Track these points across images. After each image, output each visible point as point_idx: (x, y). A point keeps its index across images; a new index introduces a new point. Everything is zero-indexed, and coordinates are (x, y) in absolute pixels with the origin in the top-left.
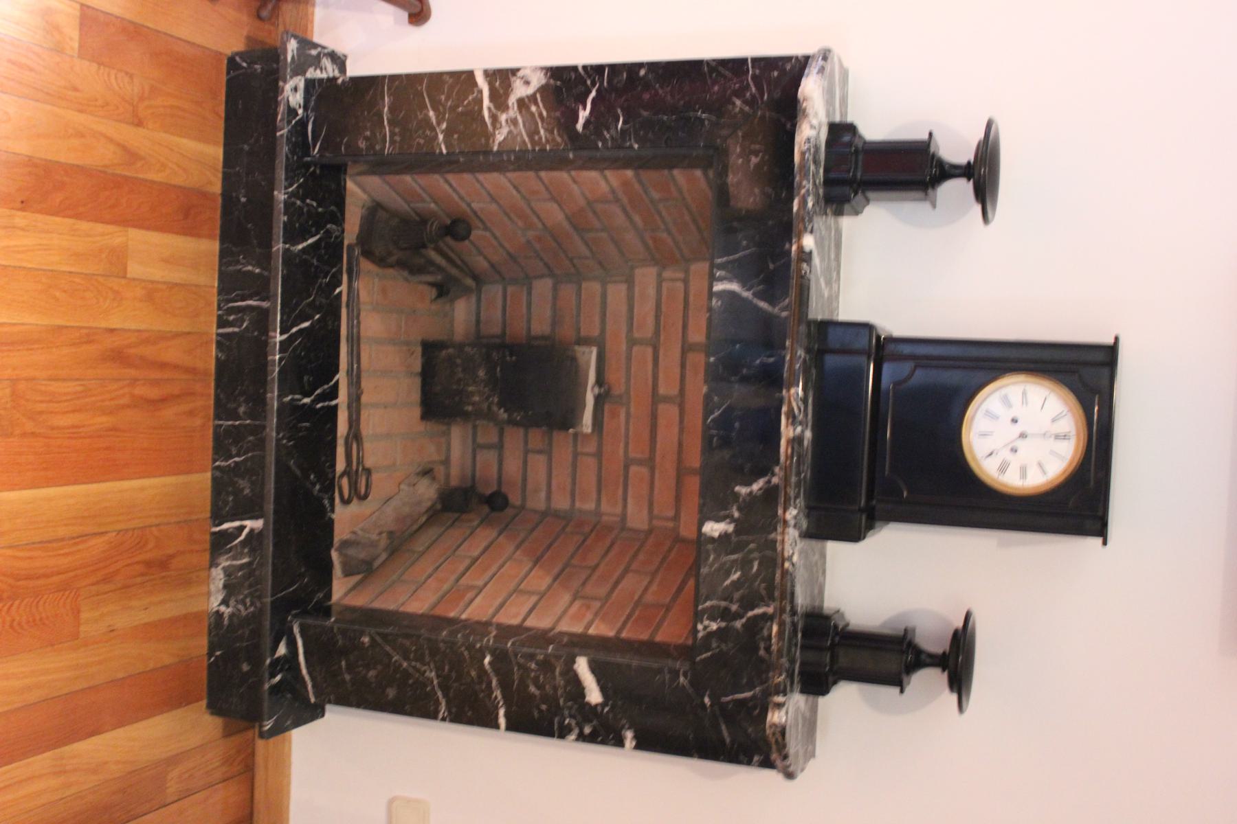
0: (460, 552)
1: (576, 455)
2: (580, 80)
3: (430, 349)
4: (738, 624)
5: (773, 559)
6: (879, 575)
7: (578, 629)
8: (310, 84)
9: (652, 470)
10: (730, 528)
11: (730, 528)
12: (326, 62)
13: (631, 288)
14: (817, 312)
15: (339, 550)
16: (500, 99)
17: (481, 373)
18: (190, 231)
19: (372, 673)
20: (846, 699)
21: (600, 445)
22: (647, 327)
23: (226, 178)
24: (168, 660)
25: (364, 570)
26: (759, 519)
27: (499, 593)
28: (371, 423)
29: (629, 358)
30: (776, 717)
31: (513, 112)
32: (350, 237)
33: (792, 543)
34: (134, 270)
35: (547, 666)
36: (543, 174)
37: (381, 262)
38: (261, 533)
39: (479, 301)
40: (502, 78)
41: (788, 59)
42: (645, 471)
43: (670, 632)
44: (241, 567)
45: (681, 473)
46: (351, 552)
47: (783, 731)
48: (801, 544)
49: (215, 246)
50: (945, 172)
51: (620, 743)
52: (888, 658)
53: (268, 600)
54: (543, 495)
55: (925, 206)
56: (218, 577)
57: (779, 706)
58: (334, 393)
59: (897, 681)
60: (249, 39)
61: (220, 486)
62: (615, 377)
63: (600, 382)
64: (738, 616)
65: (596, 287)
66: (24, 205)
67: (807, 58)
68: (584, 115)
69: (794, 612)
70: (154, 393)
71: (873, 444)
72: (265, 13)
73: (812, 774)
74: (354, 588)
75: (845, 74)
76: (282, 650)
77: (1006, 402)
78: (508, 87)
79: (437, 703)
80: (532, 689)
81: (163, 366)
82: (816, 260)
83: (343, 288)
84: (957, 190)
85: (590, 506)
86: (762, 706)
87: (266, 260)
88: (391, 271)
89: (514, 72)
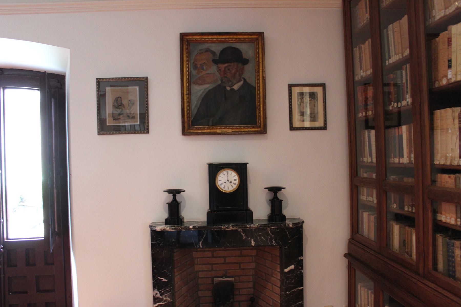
4: (273, 236)
5: (259, 229)
6: (259, 208)
7: (279, 274)
10: (252, 240)
11: (252, 240)
20: (288, 212)
22: (209, 266)
26: (249, 233)
30: (291, 225)
31: (163, 297)
33: (255, 225)
36: (176, 291)
40: (156, 300)
43: (277, 252)
47: (293, 224)
50: (175, 199)
51: (302, 260)
54: (250, 289)
57: (288, 225)
63: (222, 277)
64: (271, 236)
65: (200, 280)
67: (151, 230)
68: (164, 280)
73: (303, 218)
75: (153, 223)
78: (158, 298)
79: (299, 304)
80: (293, 281)
82: (195, 225)
84: (178, 197)
86: (288, 228)
89: (154, 297)
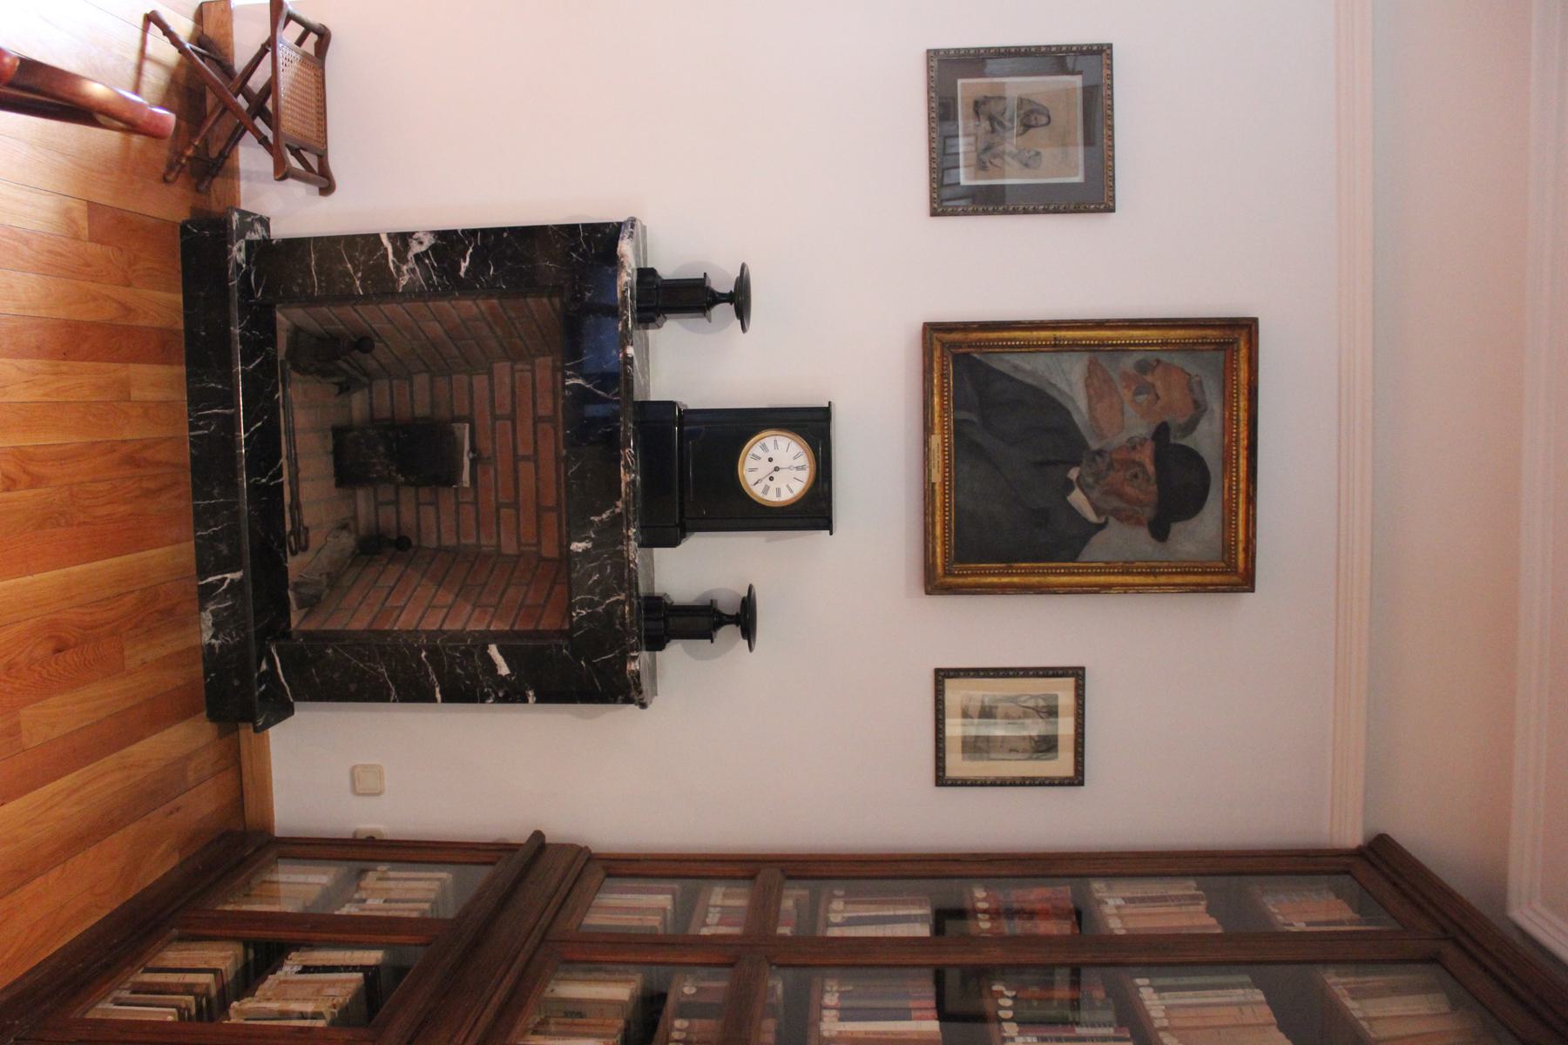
0: (380, 583)
1: (458, 504)
2: (460, 240)
3: (339, 433)
4: (600, 609)
6: (689, 568)
7: (482, 627)
8: (250, 244)
9: (518, 510)
11: (589, 545)
12: (258, 226)
13: (491, 379)
14: (638, 397)
15: (294, 590)
16: (401, 255)
17: (381, 449)
18: (165, 361)
19: (336, 675)
20: (676, 658)
21: (476, 497)
22: (507, 408)
23: (186, 317)
24: (180, 683)
25: (311, 604)
27: (423, 610)
28: (307, 492)
29: (493, 430)
30: (632, 666)
31: (412, 264)
32: (281, 355)
33: (634, 551)
34: (136, 394)
35: (468, 653)
37: (303, 371)
38: (241, 581)
39: (371, 392)
40: (402, 239)
41: (607, 225)
42: (512, 511)
44: (226, 609)
45: (540, 510)
46: (303, 590)
47: (637, 674)
48: (641, 551)
49: (181, 370)
51: (525, 701)
52: (703, 621)
53: (252, 630)
54: (435, 536)
55: (705, 320)
56: (207, 618)
57: (634, 658)
58: (279, 474)
59: (709, 635)
60: (193, 210)
61: (202, 547)
62: (485, 444)
63: (473, 449)
66: (65, 356)
67: (620, 224)
68: (464, 265)
69: (638, 597)
70: (152, 485)
71: (681, 481)
72: (202, 188)
73: (656, 705)
74: (306, 616)
75: (644, 228)
76: (264, 666)
77: (764, 447)
78: (407, 247)
79: (389, 689)
81: (158, 464)
82: (636, 362)
83: (280, 394)
84: (724, 311)
85: (472, 541)
86: (623, 659)
87: (229, 378)
88: (309, 377)
